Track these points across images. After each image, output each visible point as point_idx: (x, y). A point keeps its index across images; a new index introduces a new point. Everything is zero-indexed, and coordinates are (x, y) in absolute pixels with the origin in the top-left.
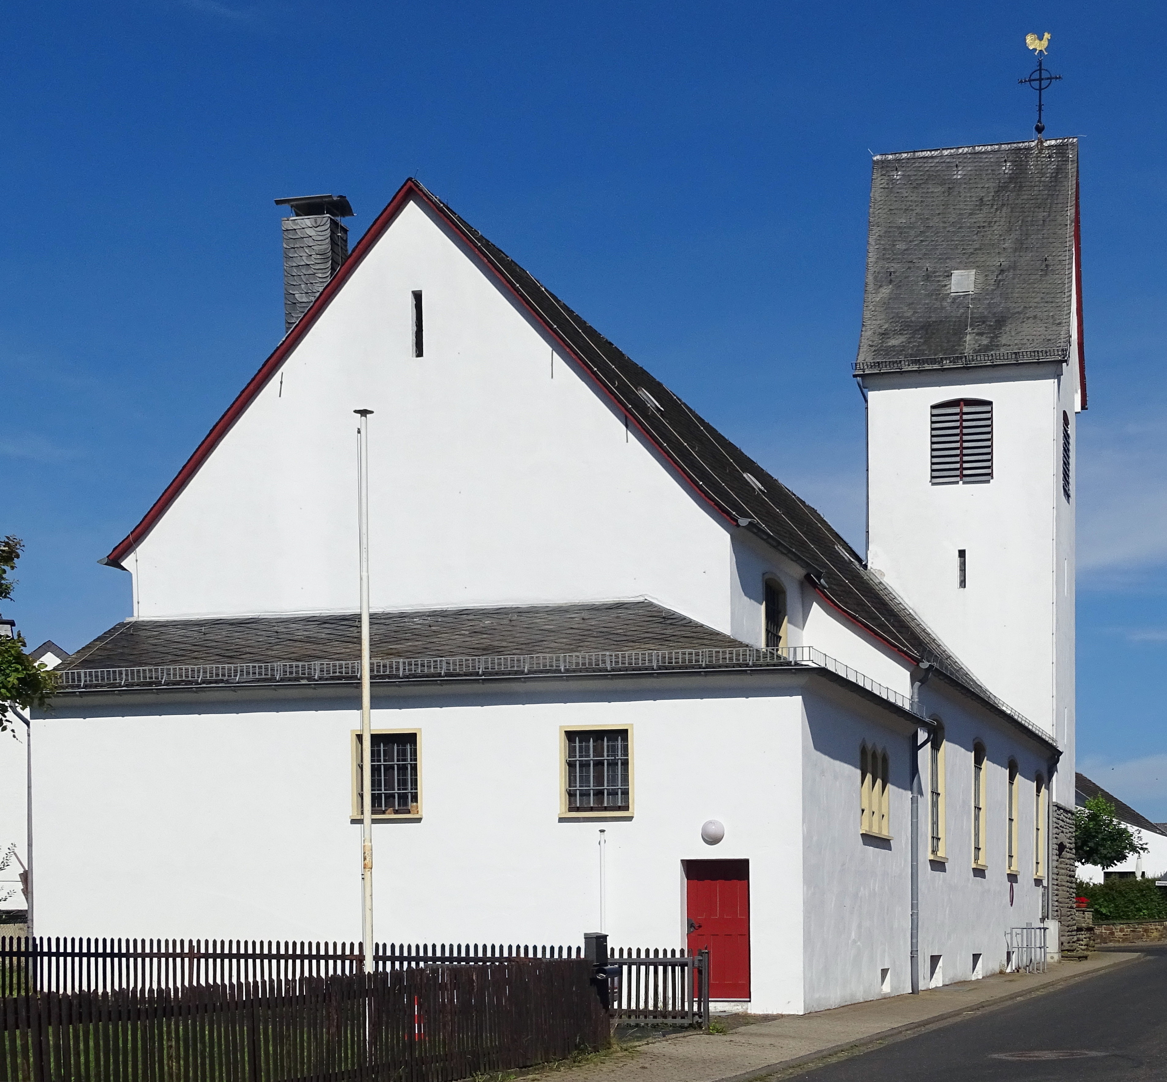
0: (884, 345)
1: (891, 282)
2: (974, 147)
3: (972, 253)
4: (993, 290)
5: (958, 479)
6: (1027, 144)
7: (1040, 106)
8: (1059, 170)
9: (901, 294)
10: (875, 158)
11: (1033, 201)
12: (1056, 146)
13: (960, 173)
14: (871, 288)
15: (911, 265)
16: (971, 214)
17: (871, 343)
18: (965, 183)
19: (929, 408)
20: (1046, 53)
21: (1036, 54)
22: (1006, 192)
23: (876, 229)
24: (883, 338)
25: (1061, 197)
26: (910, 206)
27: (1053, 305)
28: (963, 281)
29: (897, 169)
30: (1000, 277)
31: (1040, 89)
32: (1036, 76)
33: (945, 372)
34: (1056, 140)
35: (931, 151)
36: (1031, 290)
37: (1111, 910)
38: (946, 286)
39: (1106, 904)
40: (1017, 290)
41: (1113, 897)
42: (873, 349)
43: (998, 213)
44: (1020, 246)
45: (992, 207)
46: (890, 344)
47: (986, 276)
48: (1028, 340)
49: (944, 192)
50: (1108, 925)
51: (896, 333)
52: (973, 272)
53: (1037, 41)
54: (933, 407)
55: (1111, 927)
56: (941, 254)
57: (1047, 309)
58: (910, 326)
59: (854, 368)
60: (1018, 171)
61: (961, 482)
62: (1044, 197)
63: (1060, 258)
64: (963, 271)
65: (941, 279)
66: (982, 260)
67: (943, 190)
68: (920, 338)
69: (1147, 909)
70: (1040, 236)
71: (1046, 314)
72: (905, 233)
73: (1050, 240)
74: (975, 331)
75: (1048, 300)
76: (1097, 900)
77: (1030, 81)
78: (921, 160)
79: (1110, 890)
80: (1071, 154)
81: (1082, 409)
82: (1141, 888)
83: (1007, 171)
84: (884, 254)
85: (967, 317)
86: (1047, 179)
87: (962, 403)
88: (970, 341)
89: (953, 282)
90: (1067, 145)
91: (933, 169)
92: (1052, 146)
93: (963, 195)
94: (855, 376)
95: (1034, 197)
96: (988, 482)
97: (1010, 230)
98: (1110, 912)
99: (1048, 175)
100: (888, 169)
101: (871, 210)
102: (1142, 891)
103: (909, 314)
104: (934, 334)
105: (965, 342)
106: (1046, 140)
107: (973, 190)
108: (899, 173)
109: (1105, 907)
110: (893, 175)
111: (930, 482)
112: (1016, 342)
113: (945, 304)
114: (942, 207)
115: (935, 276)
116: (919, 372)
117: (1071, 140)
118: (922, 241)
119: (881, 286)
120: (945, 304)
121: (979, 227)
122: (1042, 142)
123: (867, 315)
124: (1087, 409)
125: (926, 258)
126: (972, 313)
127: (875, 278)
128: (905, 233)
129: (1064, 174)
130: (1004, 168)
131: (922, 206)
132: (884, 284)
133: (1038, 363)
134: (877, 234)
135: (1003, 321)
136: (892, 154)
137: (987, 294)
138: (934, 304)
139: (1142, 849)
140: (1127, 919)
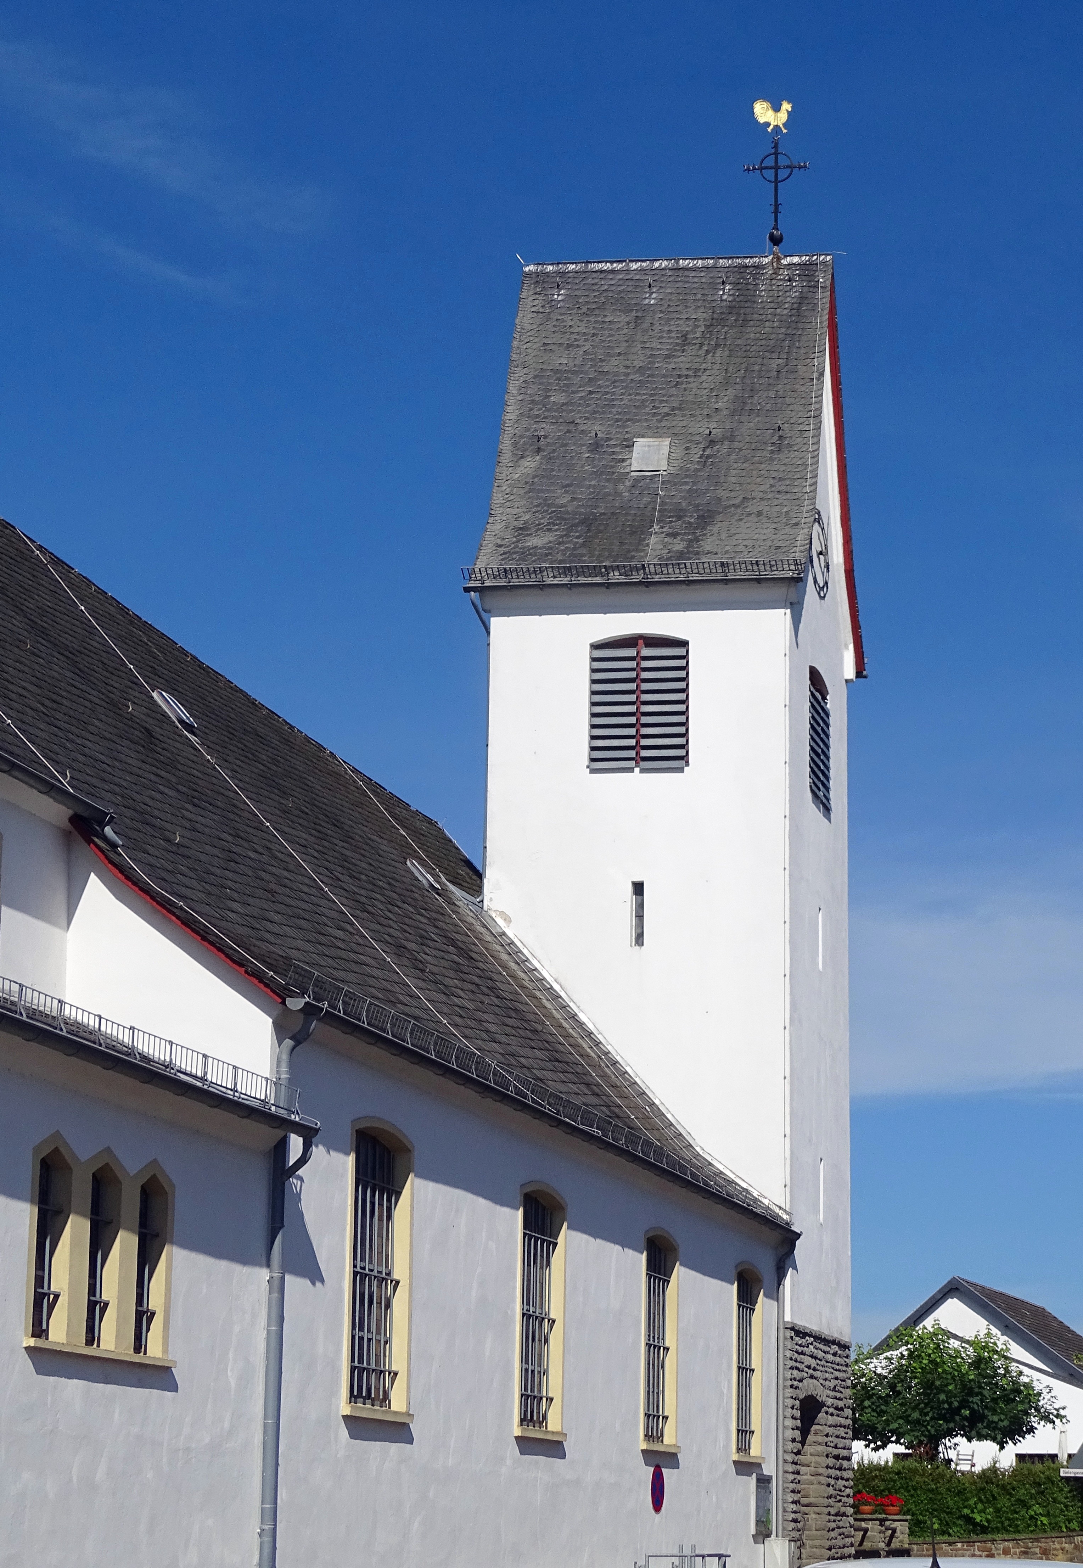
0: (520, 546)
1: (539, 450)
2: (677, 261)
3: (667, 415)
4: (696, 470)
5: (632, 764)
6: (756, 260)
7: (777, 205)
8: (802, 299)
9: (553, 470)
10: (527, 269)
11: (764, 342)
12: (799, 264)
13: (654, 296)
14: (506, 458)
15: (572, 427)
16: (668, 357)
17: (499, 542)
18: (661, 312)
19: (588, 647)
20: (785, 131)
21: (769, 130)
22: (724, 326)
23: (520, 372)
24: (519, 535)
25: (804, 338)
26: (576, 340)
27: (788, 496)
28: (650, 455)
29: (558, 286)
30: (708, 452)
31: (776, 182)
32: (770, 161)
33: (612, 590)
34: (800, 256)
35: (612, 262)
36: (755, 472)
37: (989, 1517)
38: (623, 460)
39: (980, 1506)
40: (733, 472)
41: (993, 1496)
42: (502, 550)
43: (709, 356)
44: (740, 407)
45: (700, 348)
46: (530, 544)
47: (687, 448)
48: (746, 546)
49: (628, 323)
50: (985, 1541)
51: (539, 528)
52: (667, 442)
53: (771, 112)
54: (595, 646)
55: (989, 1545)
56: (619, 413)
57: (781, 501)
58: (565, 519)
59: (467, 577)
60: (741, 298)
61: (637, 770)
62: (781, 336)
63: (801, 427)
64: (651, 440)
65: (617, 450)
66: (682, 424)
67: (627, 319)
68: (578, 537)
69: (1048, 1515)
70: (772, 394)
71: (777, 509)
72: (566, 379)
73: (788, 401)
74: (664, 530)
75: (781, 489)
76: (967, 1499)
77: (761, 169)
78: (595, 275)
79: (987, 1483)
80: (823, 278)
81: (857, 677)
82: (1037, 1480)
83: (725, 297)
84: (531, 409)
85: (654, 509)
86: (785, 312)
87: (641, 642)
88: (655, 546)
89: (635, 455)
90: (817, 264)
91: (613, 288)
92: (794, 264)
93: (657, 327)
94: (467, 590)
95: (765, 336)
96: (681, 770)
97: (726, 383)
98: (988, 1521)
99: (787, 306)
100: (546, 285)
101: (515, 343)
102: (1040, 1485)
103: (564, 501)
104: (601, 532)
105: (648, 545)
106: (786, 256)
107: (672, 322)
108: (562, 292)
109: (979, 1512)
110: (553, 295)
111: (588, 767)
112: (727, 548)
113: (621, 487)
114: (625, 344)
115: (608, 446)
116: (571, 586)
117: (822, 258)
118: (591, 392)
119: (522, 457)
120: (621, 487)
121: (679, 376)
122: (779, 259)
123: (498, 498)
124: (865, 677)
125: (595, 418)
126: (663, 503)
127: (515, 444)
128: (566, 379)
129: (810, 307)
130: (721, 293)
131: (593, 341)
132: (527, 453)
133: (758, 581)
134: (522, 379)
135: (710, 517)
136: (552, 264)
137: (687, 476)
138: (605, 487)
139: (1058, 1416)
140: (1014, 1532)
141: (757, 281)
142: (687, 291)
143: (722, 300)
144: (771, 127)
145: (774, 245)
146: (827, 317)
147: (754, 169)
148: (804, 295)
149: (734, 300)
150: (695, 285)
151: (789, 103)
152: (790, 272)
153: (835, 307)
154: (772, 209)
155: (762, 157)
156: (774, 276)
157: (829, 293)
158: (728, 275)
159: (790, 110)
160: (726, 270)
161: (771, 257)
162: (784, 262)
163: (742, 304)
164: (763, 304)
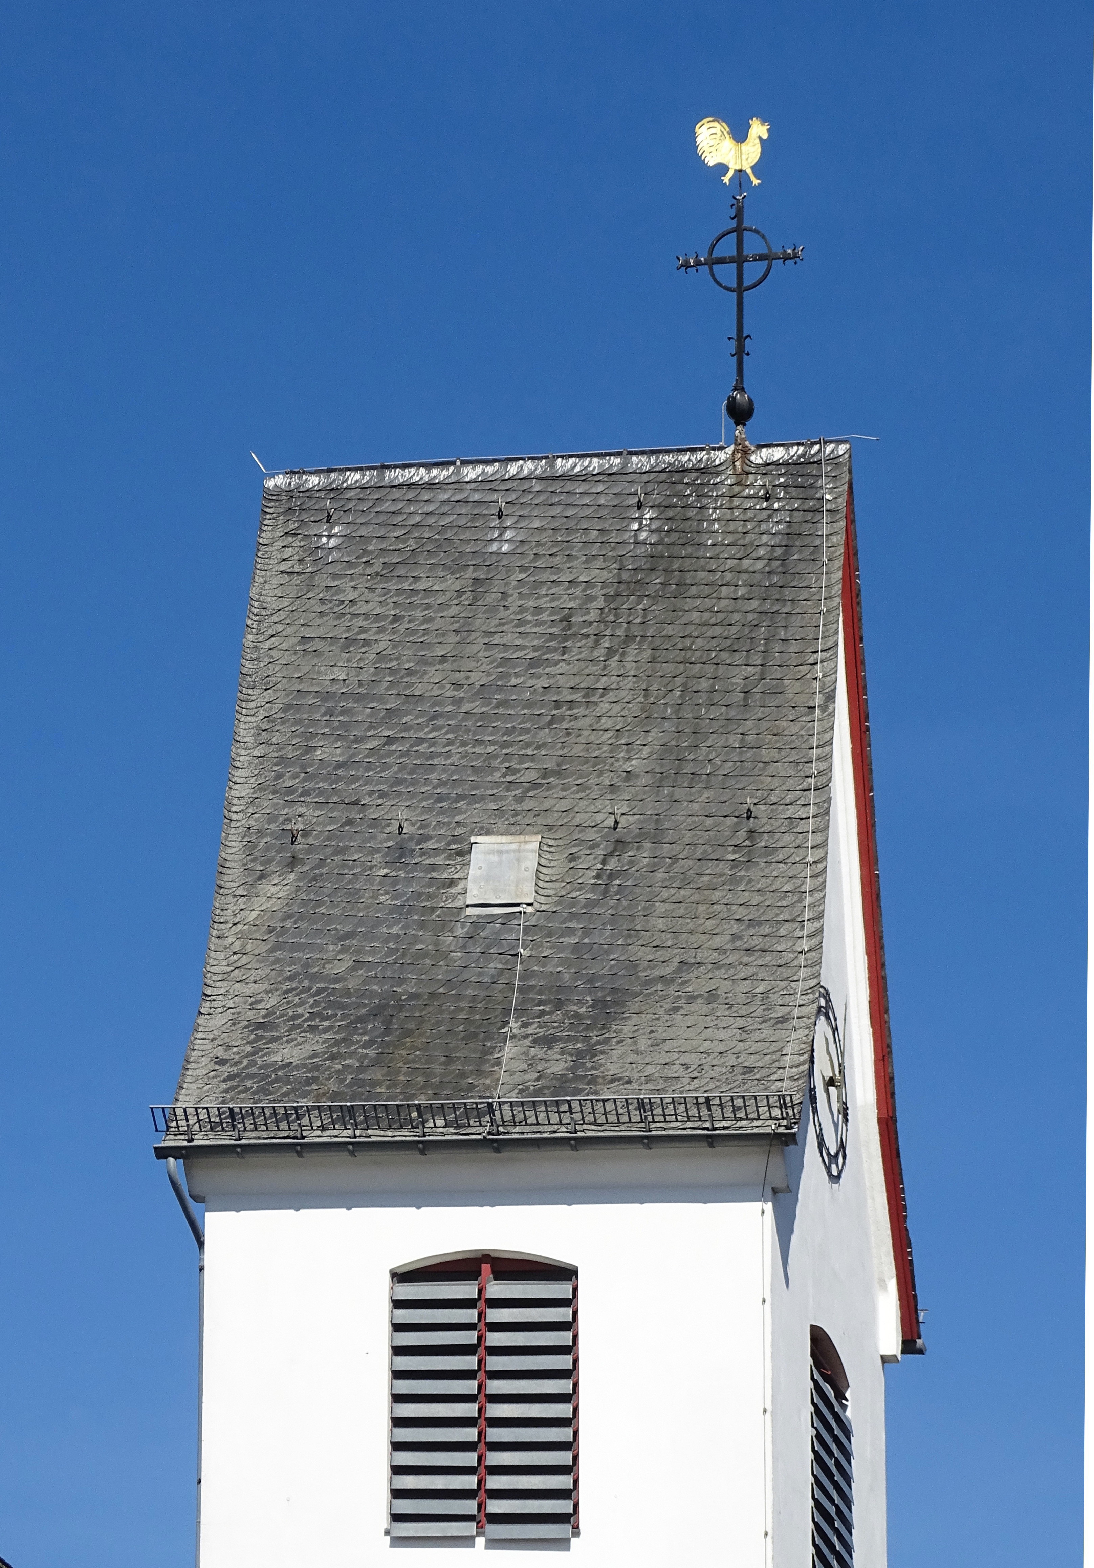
8: (792, 537)
12: (786, 464)
20: (756, 182)
21: (726, 180)
31: (740, 290)
32: (727, 248)
53: (729, 143)
60: (674, 537)
77: (712, 262)
83: (643, 536)
86: (759, 565)
90: (819, 463)
92: (776, 464)
99: (761, 552)
106: (760, 447)
117: (829, 448)
122: (746, 452)
129: (806, 553)
130: (635, 526)
141: (705, 501)
142: (572, 524)
143: (637, 543)
145: (737, 424)
147: (698, 263)
148: (795, 529)
150: (588, 512)
151: (763, 122)
152: (767, 480)
153: (856, 554)
154: (732, 346)
156: (737, 489)
157: (843, 524)
158: (649, 488)
159: (765, 136)
160: (645, 478)
161: (730, 450)
163: (676, 550)
164: (718, 549)
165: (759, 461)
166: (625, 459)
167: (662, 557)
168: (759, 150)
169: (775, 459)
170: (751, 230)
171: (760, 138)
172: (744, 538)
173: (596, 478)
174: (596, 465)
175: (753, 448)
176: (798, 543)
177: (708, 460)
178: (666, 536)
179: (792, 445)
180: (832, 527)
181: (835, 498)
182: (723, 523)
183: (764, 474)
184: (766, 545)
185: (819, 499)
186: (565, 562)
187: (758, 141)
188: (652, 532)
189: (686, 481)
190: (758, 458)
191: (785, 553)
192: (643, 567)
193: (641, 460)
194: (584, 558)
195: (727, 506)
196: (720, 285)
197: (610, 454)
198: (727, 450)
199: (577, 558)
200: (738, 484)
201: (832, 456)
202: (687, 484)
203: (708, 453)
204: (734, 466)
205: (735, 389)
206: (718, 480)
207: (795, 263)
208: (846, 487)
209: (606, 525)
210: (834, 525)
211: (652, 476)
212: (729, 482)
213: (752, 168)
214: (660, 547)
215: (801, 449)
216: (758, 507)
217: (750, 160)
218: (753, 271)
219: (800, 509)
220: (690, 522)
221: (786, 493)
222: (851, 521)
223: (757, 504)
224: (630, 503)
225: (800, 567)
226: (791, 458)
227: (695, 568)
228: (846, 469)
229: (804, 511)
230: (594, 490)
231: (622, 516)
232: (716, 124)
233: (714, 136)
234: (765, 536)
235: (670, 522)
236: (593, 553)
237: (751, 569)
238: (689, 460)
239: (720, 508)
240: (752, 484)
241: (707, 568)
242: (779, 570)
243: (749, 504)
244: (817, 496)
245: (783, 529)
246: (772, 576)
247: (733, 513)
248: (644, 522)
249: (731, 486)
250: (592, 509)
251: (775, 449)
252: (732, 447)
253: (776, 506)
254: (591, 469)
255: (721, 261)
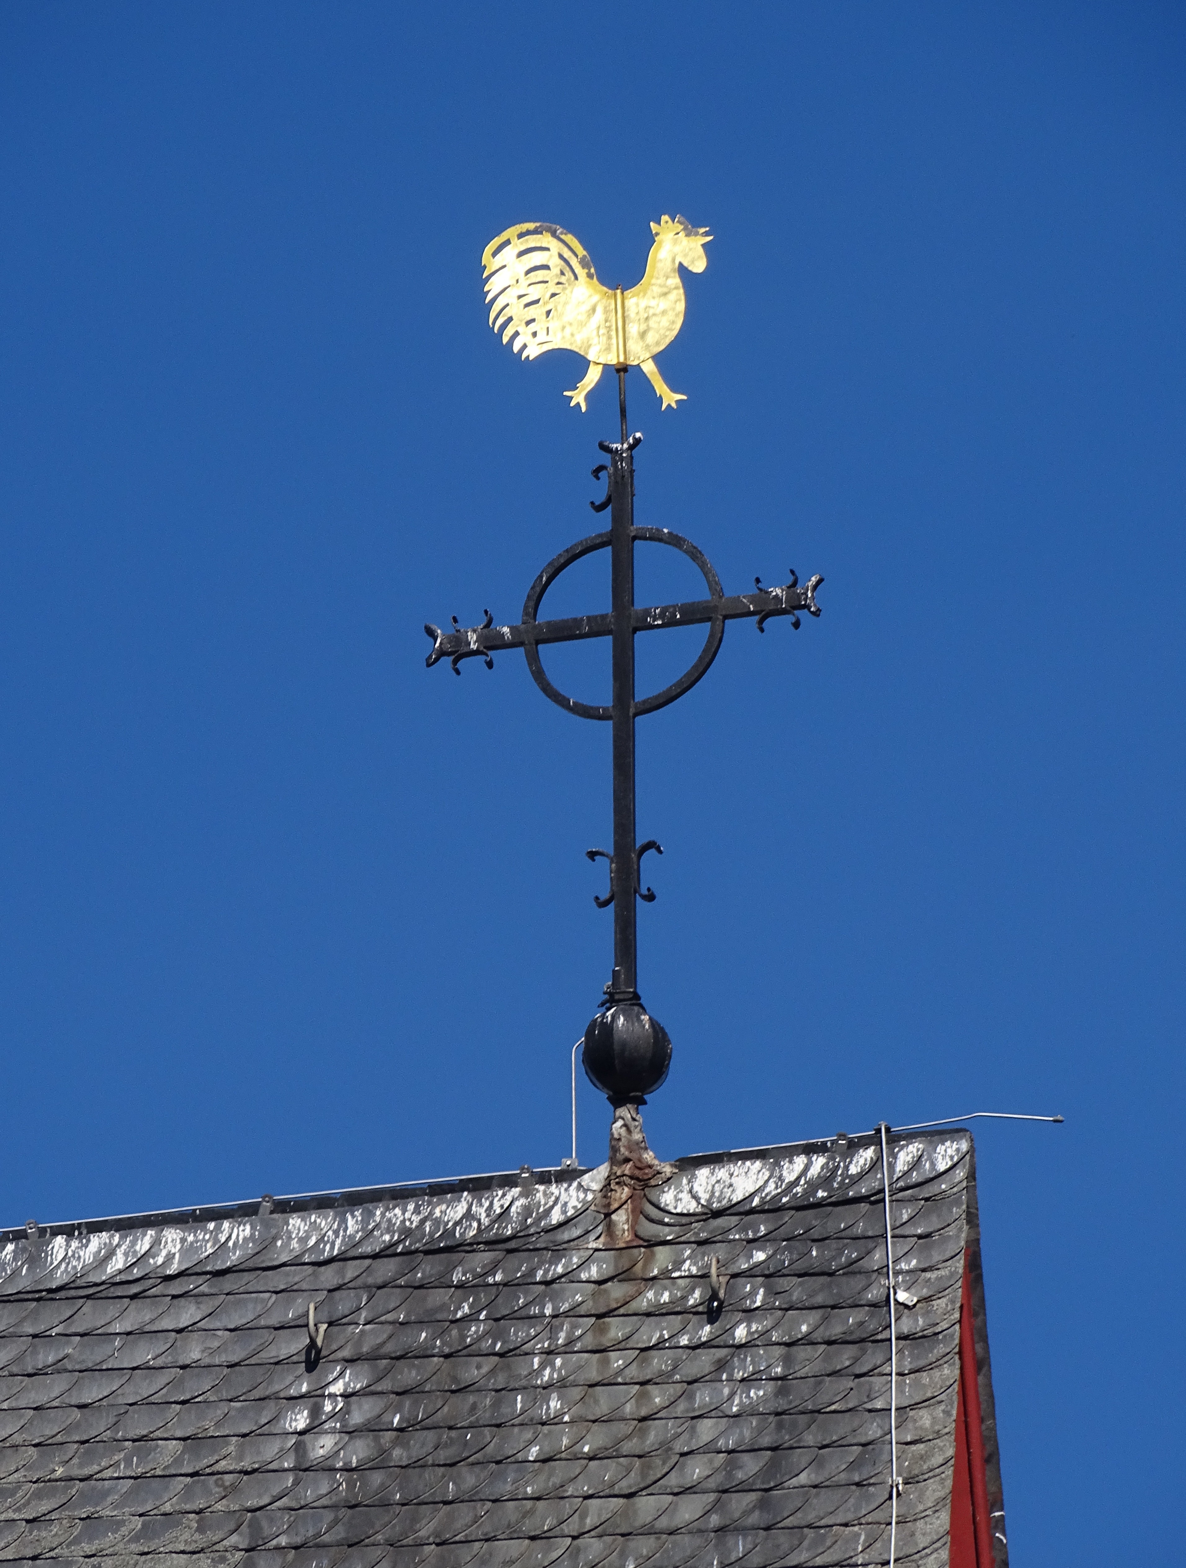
8: (792, 1420)
12: (771, 1209)
20: (670, 398)
21: (578, 397)
31: (624, 713)
32: (586, 591)
53: (584, 294)
60: (421, 1444)
77: (534, 638)
83: (323, 1446)
86: (689, 1510)
90: (875, 1199)
92: (741, 1210)
99: (696, 1470)
106: (688, 1164)
117: (905, 1156)
122: (644, 1183)
129: (837, 1465)
130: (301, 1421)
141: (517, 1333)
142: (99, 1426)
143: (303, 1469)
144: (593, 376)
145: (617, 1101)
146: (943, 1520)
147: (492, 643)
148: (801, 1395)
149: (378, 1462)
150: (145, 1387)
151: (692, 224)
152: (711, 1259)
153: (992, 1458)
154: (601, 878)
155: (538, 566)
156: (617, 1291)
157: (950, 1372)
158: (343, 1304)
159: (699, 266)
160: (329, 1276)
161: (594, 1180)
162: (677, 1199)
163: (426, 1483)
164: (560, 1471)
165: (688, 1205)
166: (266, 1225)
167: (385, 1504)
168: (681, 306)
169: (738, 1196)
170: (656, 537)
171: (683, 271)
172: (643, 1434)
173: (175, 1288)
174: (176, 1249)
175: (668, 1170)
176: (809, 1439)
177: (527, 1211)
178: (395, 1443)
179: (790, 1153)
180: (916, 1384)
181: (927, 1299)
182: (576, 1393)
183: (700, 1243)
184: (710, 1449)
185: (874, 1305)
186: (76, 1541)
187: (676, 281)
188: (351, 1433)
189: (457, 1276)
190: (685, 1196)
191: (772, 1468)
192: (326, 1538)
193: (314, 1226)
194: (138, 1523)
195: (589, 1341)
196: (560, 700)
197: (218, 1215)
198: (586, 1179)
199: (116, 1524)
200: (622, 1276)
201: (915, 1177)
202: (461, 1286)
203: (525, 1194)
204: (610, 1228)
205: (611, 1000)
206: (560, 1269)
207: (797, 625)
208: (959, 1265)
209: (207, 1424)
210: (924, 1378)
211: (352, 1270)
212: (594, 1272)
213: (657, 358)
214: (377, 1478)
215: (819, 1162)
216: (684, 1341)
217: (651, 338)
218: (661, 658)
219: (817, 1336)
220: (471, 1399)
221: (772, 1293)
222: (974, 1361)
223: (682, 1331)
224: (283, 1353)
225: (819, 1507)
226: (785, 1193)
227: (487, 1528)
228: (958, 1211)
229: (830, 1343)
230: (167, 1323)
231: (256, 1394)
232: (546, 240)
233: (540, 275)
234: (708, 1423)
235: (407, 1403)
236: (167, 1508)
237: (663, 1523)
238: (468, 1215)
239: (567, 1349)
240: (665, 1275)
241: (528, 1527)
242: (754, 1518)
243: (653, 1333)
244: (871, 1295)
245: (764, 1400)
246: (730, 1540)
247: (606, 1362)
248: (328, 1407)
249: (599, 1283)
250: (163, 1378)
251: (738, 1168)
252: (603, 1170)
253: (741, 1333)
254: (160, 1260)
255: (565, 632)
